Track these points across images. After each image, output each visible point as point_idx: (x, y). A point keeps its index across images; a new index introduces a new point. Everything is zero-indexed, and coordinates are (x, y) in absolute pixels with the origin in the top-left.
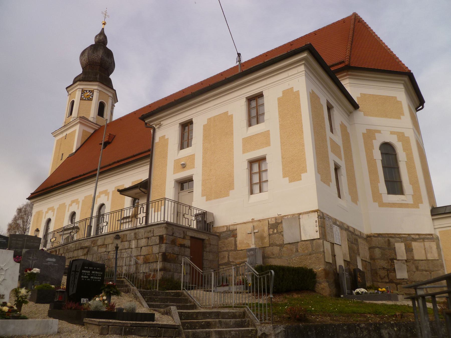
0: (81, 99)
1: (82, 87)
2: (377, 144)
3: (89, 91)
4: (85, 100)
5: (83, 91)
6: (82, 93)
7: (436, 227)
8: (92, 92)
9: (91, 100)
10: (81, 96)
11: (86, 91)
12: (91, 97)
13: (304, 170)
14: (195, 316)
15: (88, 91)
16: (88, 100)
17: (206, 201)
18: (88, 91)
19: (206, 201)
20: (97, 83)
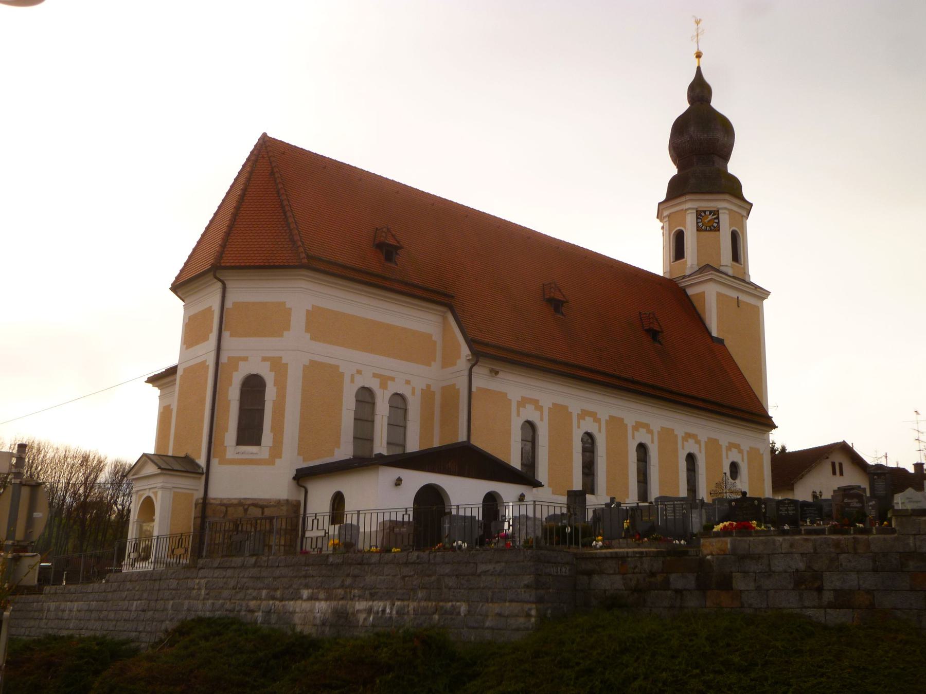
0: (699, 229)
1: (696, 205)
2: (237, 379)
3: (711, 212)
4: (706, 230)
5: (700, 214)
6: (697, 218)
7: (362, 516)
8: (716, 213)
9: (717, 229)
10: (697, 223)
11: (705, 212)
12: (715, 225)
13: (211, 332)
14: (588, 454)
15: (708, 213)
16: (711, 230)
17: (443, 367)
18: (708, 213)
19: (443, 367)
20: (688, 197)
